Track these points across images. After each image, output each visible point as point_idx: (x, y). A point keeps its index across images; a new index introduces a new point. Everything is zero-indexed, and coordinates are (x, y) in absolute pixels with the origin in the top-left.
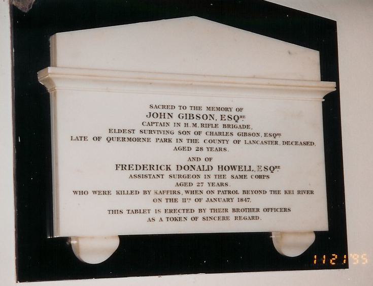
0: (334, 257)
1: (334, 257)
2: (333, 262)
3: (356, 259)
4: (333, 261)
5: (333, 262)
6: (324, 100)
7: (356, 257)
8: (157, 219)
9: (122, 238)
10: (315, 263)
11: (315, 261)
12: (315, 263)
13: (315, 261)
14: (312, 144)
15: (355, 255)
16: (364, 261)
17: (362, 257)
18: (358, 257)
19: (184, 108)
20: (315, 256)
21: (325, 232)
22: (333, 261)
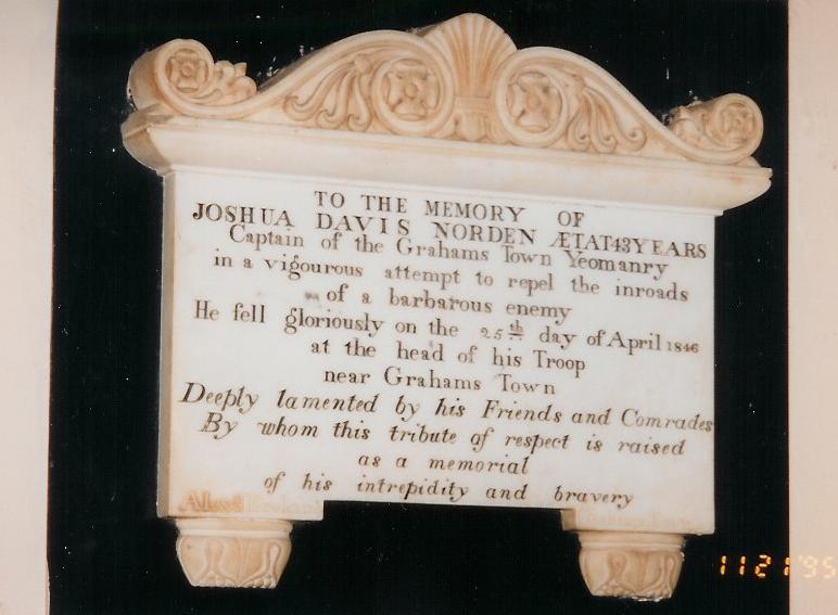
0: (764, 561)
1: (764, 561)
2: (761, 572)
3: (810, 567)
4: (762, 570)
5: (761, 572)
6: (697, 102)
7: (810, 562)
8: (238, 261)
9: (329, 507)
10: (723, 572)
11: (723, 568)
12: (723, 572)
13: (723, 568)
14: (406, 498)
15: (811, 558)
16: (829, 572)
17: (825, 563)
18: (816, 562)
19: (338, 200)
20: (743, 558)
21: (316, 522)
22: (762, 570)
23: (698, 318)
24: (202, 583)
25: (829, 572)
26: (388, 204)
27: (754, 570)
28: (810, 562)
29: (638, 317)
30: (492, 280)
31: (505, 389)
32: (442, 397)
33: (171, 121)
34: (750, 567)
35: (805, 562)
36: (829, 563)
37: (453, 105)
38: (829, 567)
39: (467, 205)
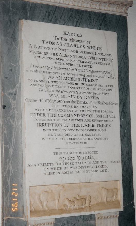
0: (14, 194)
4: (14, 194)
17: (16, 208)
23: (115, 82)
24: (108, 33)
25: (14, 209)
26: (96, 77)
27: (14, 192)
28: (16, 205)
29: (107, 99)
30: (59, 39)
31: (55, 39)
32: (93, 156)
33: (61, 209)
34: (14, 191)
35: (16, 204)
36: (16, 210)
37: (106, 218)
38: (15, 210)
39: (72, 39)
